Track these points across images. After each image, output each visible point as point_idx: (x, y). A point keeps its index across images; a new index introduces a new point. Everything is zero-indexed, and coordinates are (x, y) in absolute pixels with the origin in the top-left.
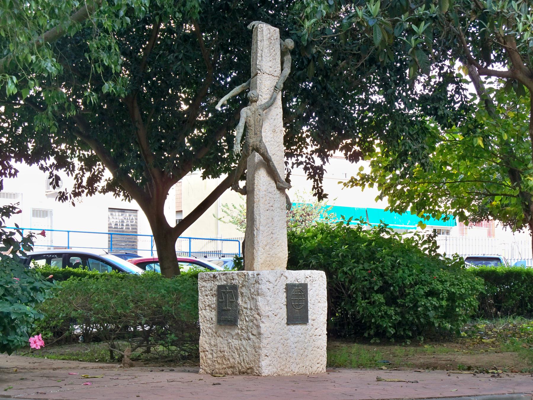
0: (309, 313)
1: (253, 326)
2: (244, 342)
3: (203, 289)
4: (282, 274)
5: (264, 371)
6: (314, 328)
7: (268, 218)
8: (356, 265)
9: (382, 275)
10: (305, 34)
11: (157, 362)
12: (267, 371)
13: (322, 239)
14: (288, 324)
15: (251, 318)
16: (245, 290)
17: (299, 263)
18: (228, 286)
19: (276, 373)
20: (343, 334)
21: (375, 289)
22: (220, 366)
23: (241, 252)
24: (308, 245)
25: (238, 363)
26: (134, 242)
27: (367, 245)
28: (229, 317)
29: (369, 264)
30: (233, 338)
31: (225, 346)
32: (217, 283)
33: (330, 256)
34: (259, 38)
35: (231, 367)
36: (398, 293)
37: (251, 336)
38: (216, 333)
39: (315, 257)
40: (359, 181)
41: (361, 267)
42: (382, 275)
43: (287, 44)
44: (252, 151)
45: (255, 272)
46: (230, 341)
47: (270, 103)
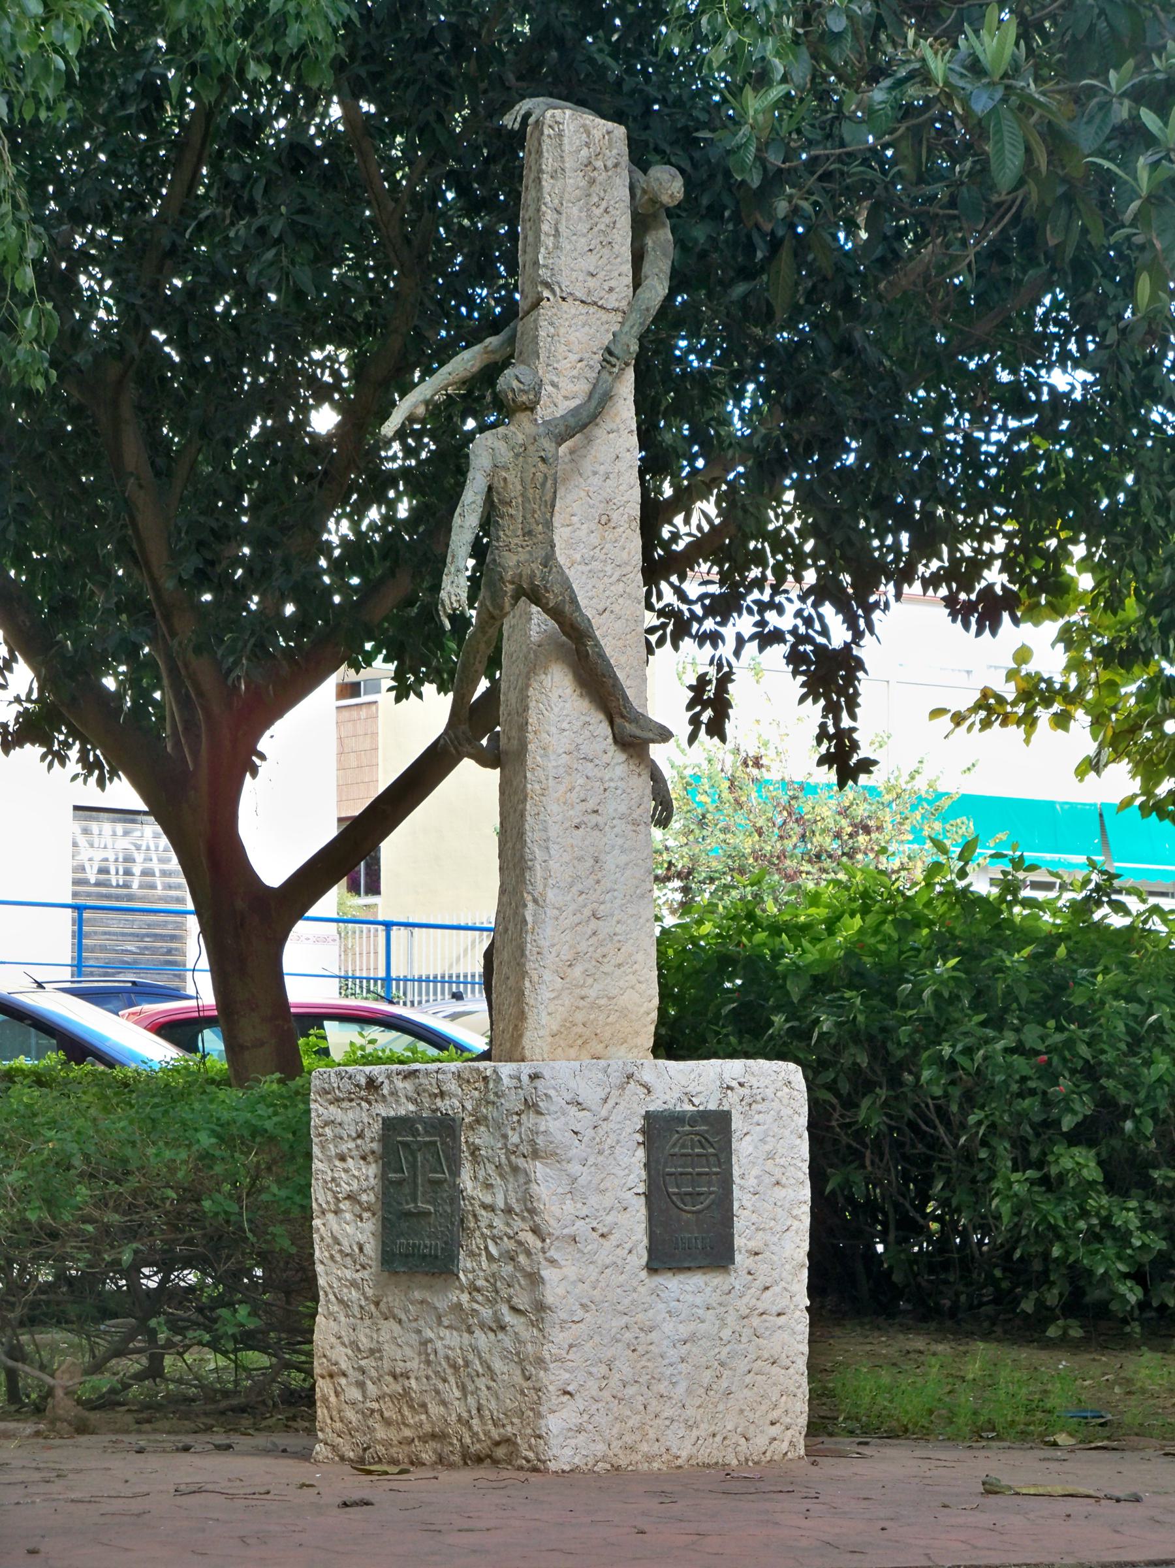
0: (739, 1225)
1: (512, 1276)
2: (483, 1340)
3: (327, 1130)
4: (630, 1076)
5: (555, 1451)
6: (758, 1284)
7: (580, 859)
8: (990, 1033)
9: (1091, 1072)
10: (744, 146)
11: (185, 1416)
12: (568, 1452)
13: (861, 931)
14: (653, 1268)
15: (509, 1244)
16: (486, 1135)
17: (771, 1024)
18: (421, 1119)
19: (604, 1459)
20: (947, 1303)
21: (1065, 1129)
22: (392, 1434)
24: (809, 958)
25: (460, 1419)
26: (173, 938)
27: (1035, 957)
28: (427, 1243)
29: (1039, 1030)
30: (440, 1323)
31: (408, 1352)
32: (383, 1111)
33: (891, 1000)
34: (549, 162)
35: (434, 1436)
36: (1153, 1144)
37: (509, 1318)
38: (377, 1304)
39: (831, 1004)
40: (1014, 704)
41: (1009, 1039)
42: (1091, 1072)
43: (655, 186)
44: (516, 598)
45: (526, 1069)
46: (430, 1334)
47: (584, 414)
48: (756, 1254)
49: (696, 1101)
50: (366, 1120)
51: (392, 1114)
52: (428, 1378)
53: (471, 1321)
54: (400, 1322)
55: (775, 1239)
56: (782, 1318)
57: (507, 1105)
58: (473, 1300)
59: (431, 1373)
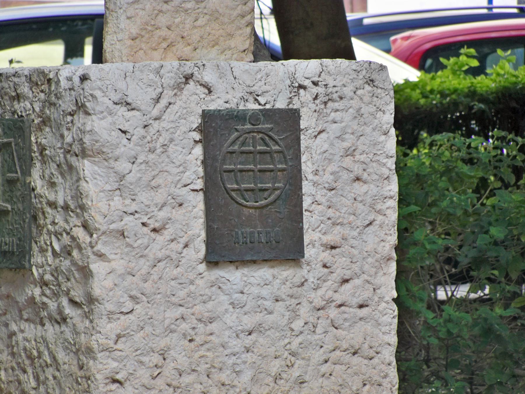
6: (336, 276)
16: (49, 136)
23: (495, 11)
37: (68, 310)
46: (14, 327)
48: (333, 248)
49: (262, 100)
52: (13, 369)
55: (355, 233)
56: (365, 310)
57: (64, 106)
58: (43, 294)
59: (15, 365)
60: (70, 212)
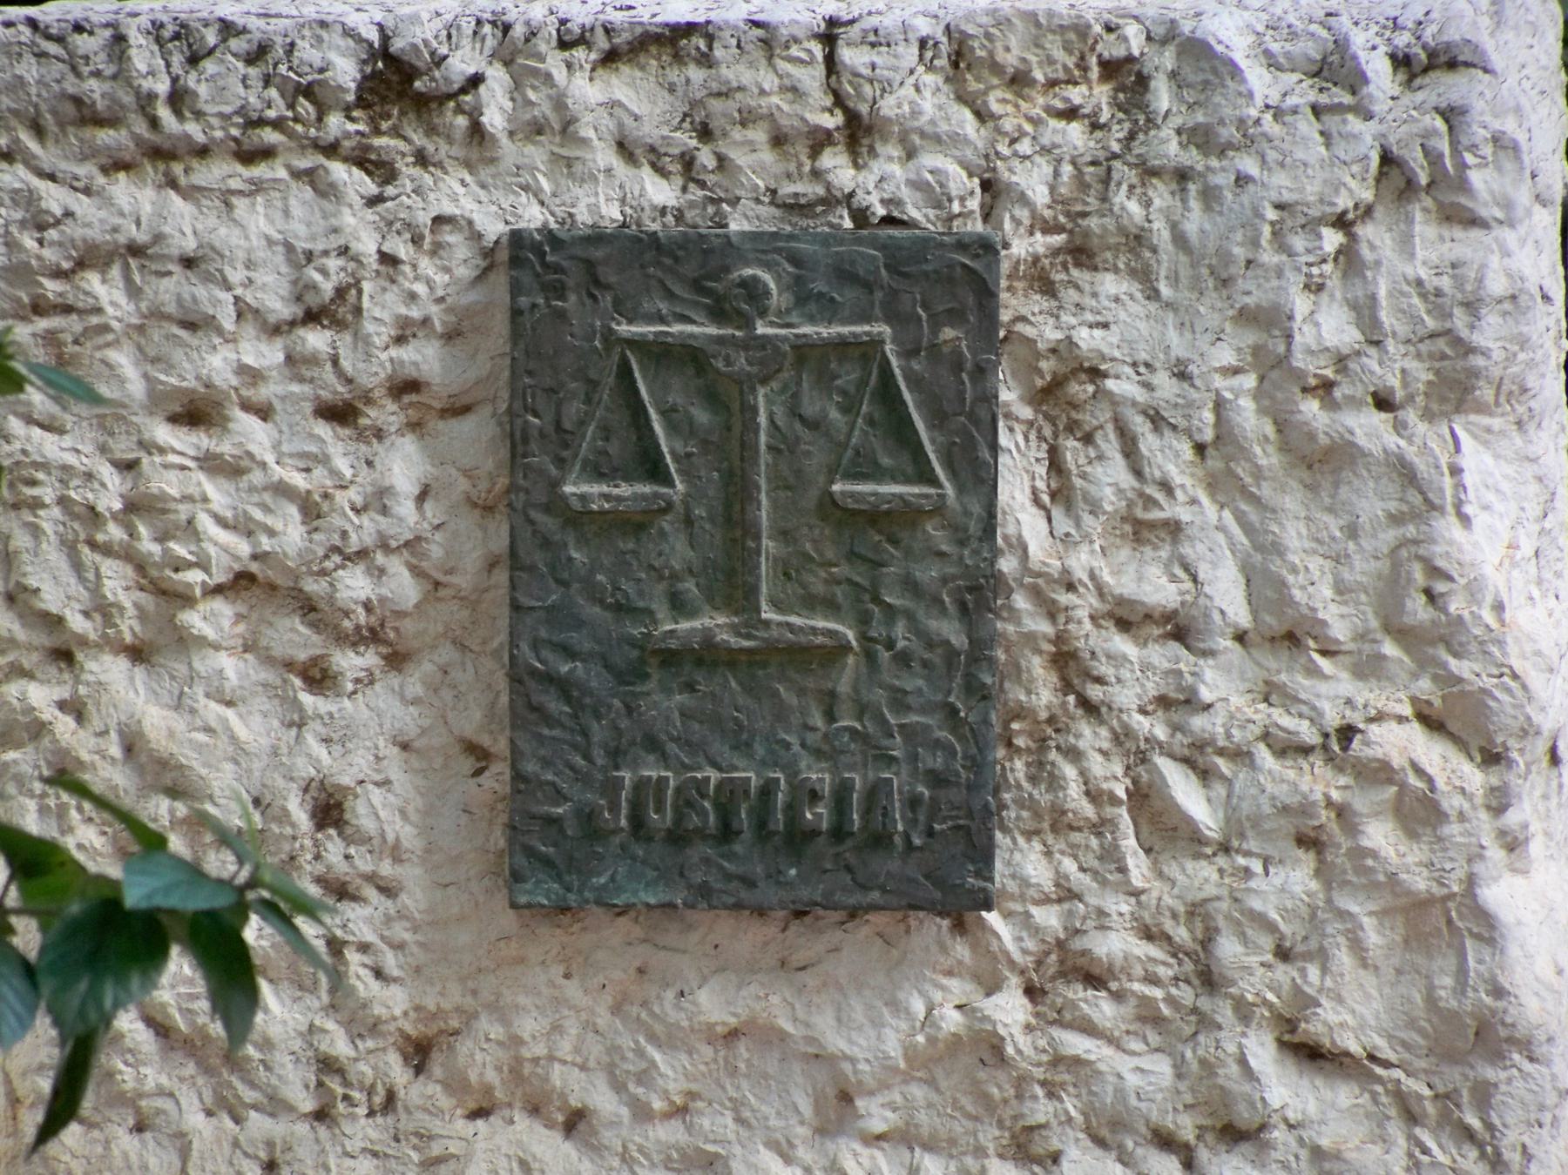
38: (419, 1053)
50: (368, 245)
51: (533, 216)
53: (1041, 1110)
54: (575, 1122)
57: (1281, 184)
60: (1316, 656)
